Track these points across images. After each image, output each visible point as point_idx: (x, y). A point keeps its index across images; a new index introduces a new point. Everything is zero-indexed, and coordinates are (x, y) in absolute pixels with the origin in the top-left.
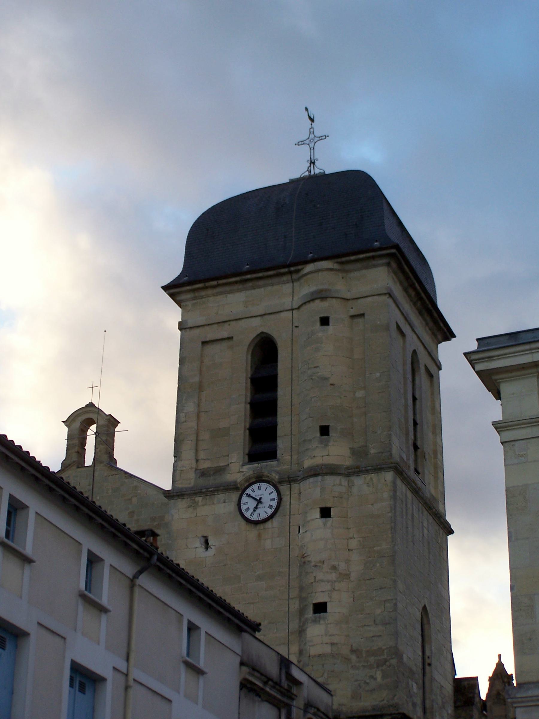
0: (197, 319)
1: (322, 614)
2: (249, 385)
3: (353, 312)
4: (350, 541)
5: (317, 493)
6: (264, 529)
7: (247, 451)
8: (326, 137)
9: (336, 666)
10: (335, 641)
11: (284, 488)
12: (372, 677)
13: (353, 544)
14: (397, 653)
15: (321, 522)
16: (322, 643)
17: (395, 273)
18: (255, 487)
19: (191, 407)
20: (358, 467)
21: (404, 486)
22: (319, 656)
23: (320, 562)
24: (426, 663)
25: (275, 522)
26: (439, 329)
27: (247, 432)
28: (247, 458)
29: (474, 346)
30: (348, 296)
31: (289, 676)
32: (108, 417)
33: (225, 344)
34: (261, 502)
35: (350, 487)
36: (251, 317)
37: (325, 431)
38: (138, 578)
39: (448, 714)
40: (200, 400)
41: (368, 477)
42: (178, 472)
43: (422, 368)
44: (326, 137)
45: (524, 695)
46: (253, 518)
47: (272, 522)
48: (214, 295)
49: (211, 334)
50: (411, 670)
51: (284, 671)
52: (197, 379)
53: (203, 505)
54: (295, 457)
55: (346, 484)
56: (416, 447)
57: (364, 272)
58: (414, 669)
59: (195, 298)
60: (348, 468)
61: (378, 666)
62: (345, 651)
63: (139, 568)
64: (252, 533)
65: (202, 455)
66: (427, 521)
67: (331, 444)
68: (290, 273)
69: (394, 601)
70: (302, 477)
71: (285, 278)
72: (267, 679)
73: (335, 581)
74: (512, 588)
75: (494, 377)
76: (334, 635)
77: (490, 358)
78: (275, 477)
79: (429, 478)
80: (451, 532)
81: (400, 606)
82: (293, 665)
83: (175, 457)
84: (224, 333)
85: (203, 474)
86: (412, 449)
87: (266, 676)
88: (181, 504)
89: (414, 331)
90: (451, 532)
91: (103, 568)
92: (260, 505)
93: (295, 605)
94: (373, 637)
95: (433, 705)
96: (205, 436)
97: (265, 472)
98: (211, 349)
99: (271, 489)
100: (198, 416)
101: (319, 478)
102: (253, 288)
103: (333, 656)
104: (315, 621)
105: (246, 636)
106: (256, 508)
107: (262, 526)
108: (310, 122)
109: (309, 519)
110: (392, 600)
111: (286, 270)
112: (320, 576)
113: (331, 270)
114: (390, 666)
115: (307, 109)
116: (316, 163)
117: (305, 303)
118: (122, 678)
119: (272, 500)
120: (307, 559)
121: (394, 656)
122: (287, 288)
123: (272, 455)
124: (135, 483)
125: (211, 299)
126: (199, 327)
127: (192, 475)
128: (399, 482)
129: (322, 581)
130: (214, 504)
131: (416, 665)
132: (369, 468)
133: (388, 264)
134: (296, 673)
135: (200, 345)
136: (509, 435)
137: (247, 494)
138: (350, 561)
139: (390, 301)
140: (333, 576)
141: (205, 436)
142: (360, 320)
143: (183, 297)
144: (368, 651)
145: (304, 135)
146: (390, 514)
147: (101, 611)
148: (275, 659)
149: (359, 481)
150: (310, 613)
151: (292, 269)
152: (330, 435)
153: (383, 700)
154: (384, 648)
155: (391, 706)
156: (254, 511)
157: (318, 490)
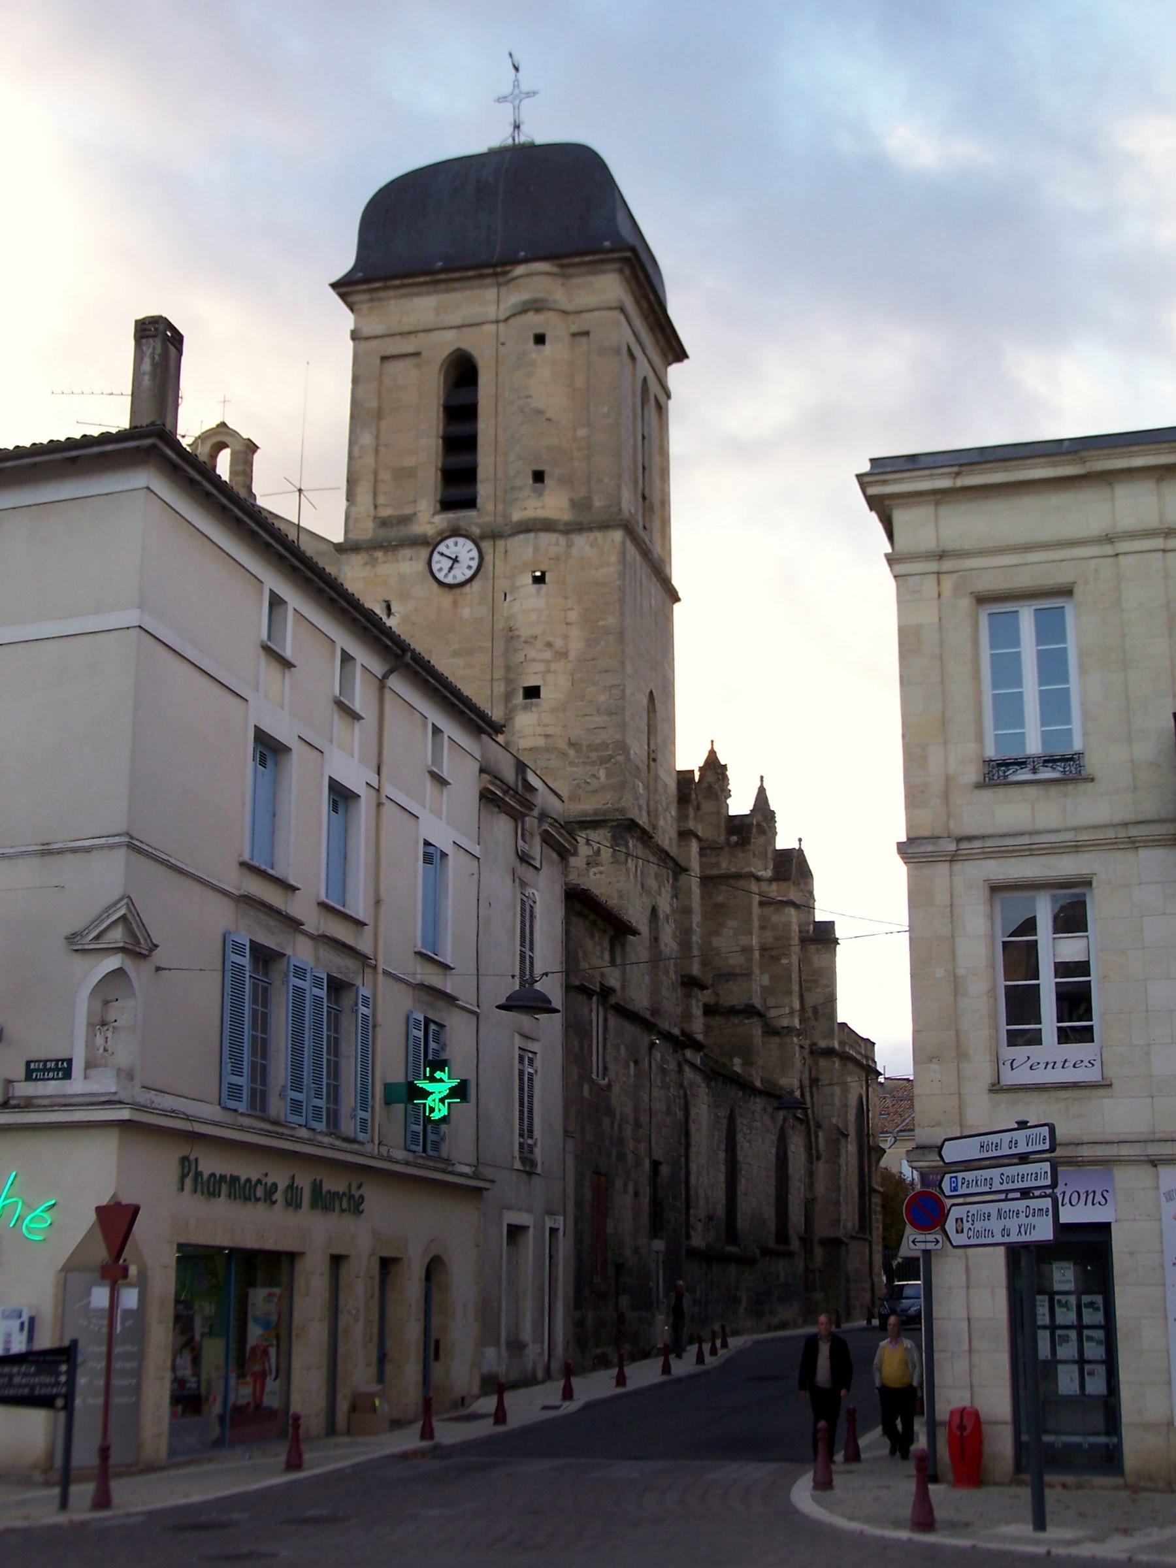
0: (373, 326)
1: (534, 700)
2: (441, 415)
3: (574, 328)
4: (569, 613)
5: (528, 554)
6: (461, 594)
7: (439, 498)
8: (535, 93)
9: (551, 761)
10: (549, 733)
11: (486, 545)
12: (594, 776)
13: (573, 616)
14: (623, 747)
15: (533, 588)
16: (534, 735)
17: (628, 281)
18: (450, 542)
19: (367, 439)
20: (580, 523)
21: (633, 547)
22: (531, 749)
23: (532, 637)
24: (652, 758)
25: (476, 585)
26: (672, 348)
27: (439, 473)
28: (438, 506)
29: (866, 467)
30: (569, 307)
31: (525, 781)
32: (247, 441)
33: (409, 362)
34: (458, 561)
35: (570, 545)
37: (539, 477)
38: (387, 678)
39: (672, 817)
40: (378, 431)
41: (592, 536)
43: (652, 398)
44: (535, 93)
45: (916, 851)
46: (447, 581)
47: (471, 587)
48: (397, 297)
50: (637, 767)
51: (520, 777)
52: (374, 404)
53: (384, 562)
54: (500, 507)
55: (564, 544)
56: (644, 498)
57: (590, 278)
58: (641, 765)
59: (371, 300)
60: (566, 524)
61: (601, 764)
62: (562, 744)
63: (386, 668)
64: (446, 599)
65: (382, 500)
66: (655, 588)
67: (547, 492)
68: (496, 275)
69: (621, 688)
70: (509, 533)
71: (488, 281)
72: (507, 788)
73: (550, 661)
74: (904, 736)
75: (887, 502)
76: (548, 726)
77: (885, 482)
78: (476, 531)
79: (657, 536)
80: (678, 599)
81: (628, 692)
82: (528, 769)
83: (348, 500)
84: (409, 346)
85: (384, 523)
86: (641, 500)
87: (507, 785)
88: (357, 560)
89: (645, 353)
90: (678, 599)
91: (355, 667)
92: (456, 565)
93: (500, 688)
94: (595, 728)
95: (657, 807)
96: (385, 476)
97: (463, 524)
98: (393, 367)
99: (470, 545)
100: (377, 451)
101: (532, 535)
102: (448, 291)
103: (547, 750)
104: (526, 708)
105: (484, 737)
106: (451, 568)
107: (458, 591)
108: (513, 71)
109: (518, 584)
110: (619, 685)
111: (491, 271)
112: (532, 654)
113: (549, 274)
114: (615, 764)
115: (511, 55)
116: (522, 127)
117: (514, 315)
118: (373, 793)
119: (472, 559)
120: (517, 633)
121: (621, 752)
122: (491, 294)
123: (470, 503)
125: (393, 302)
126: (376, 337)
127: (370, 525)
128: (629, 544)
129: (534, 660)
130: (397, 561)
131: (642, 761)
132: (592, 525)
133: (621, 271)
134: (532, 779)
135: (378, 361)
136: (902, 568)
137: (439, 553)
139: (622, 318)
140: (548, 655)
141: (385, 476)
142: (584, 340)
143: (354, 298)
144: (589, 746)
145: (507, 89)
146: (618, 583)
147: (354, 718)
148: (512, 761)
149: (581, 541)
150: (519, 698)
151: (499, 270)
152: (546, 482)
153: (608, 803)
154: (609, 742)
155: (618, 810)
156: (449, 572)
157: (531, 550)
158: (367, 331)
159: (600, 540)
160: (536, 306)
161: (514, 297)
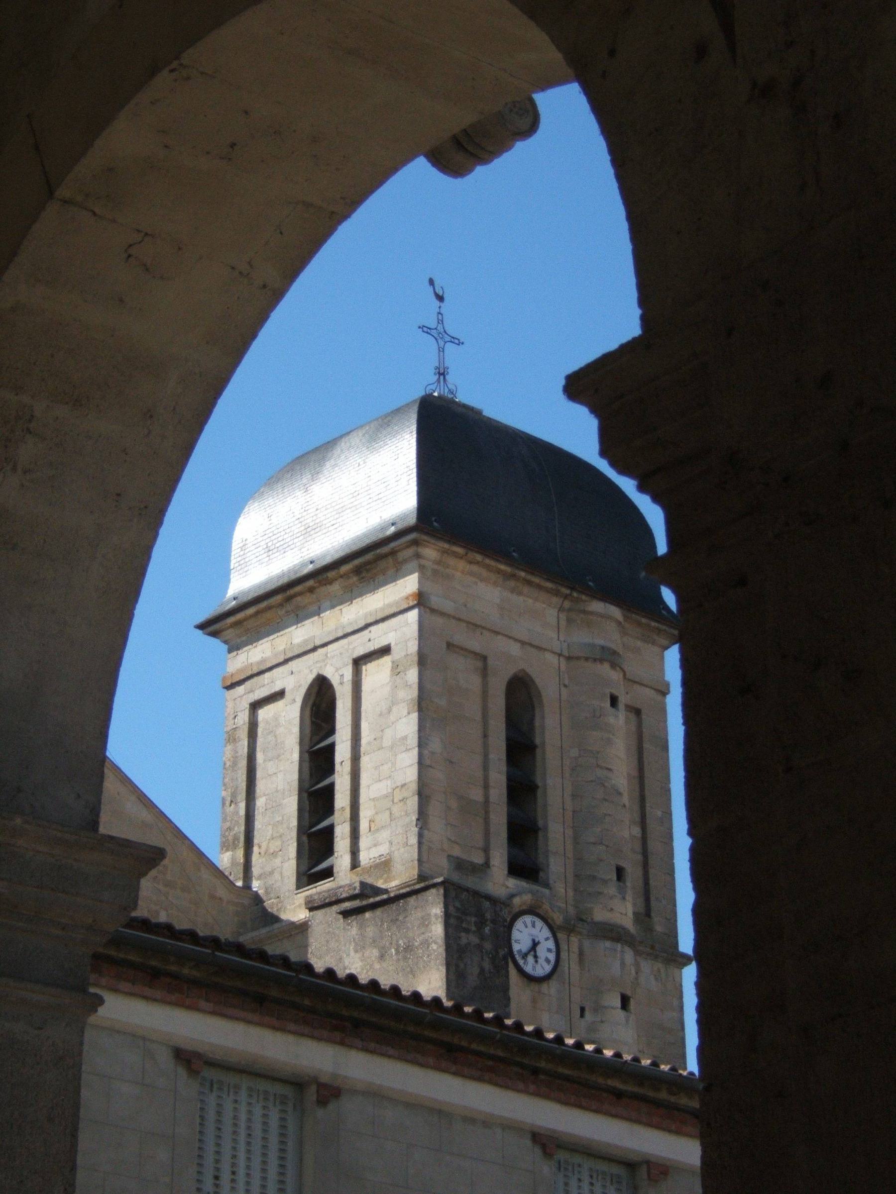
19: (436, 745)
36: (510, 638)
42: (425, 848)
44: (460, 343)
49: (461, 637)
78: (558, 918)
99: (546, 932)
101: (619, 946)
107: (534, 986)
108: (437, 303)
115: (431, 282)
158: (435, 601)
160: (609, 657)
161: (582, 637)
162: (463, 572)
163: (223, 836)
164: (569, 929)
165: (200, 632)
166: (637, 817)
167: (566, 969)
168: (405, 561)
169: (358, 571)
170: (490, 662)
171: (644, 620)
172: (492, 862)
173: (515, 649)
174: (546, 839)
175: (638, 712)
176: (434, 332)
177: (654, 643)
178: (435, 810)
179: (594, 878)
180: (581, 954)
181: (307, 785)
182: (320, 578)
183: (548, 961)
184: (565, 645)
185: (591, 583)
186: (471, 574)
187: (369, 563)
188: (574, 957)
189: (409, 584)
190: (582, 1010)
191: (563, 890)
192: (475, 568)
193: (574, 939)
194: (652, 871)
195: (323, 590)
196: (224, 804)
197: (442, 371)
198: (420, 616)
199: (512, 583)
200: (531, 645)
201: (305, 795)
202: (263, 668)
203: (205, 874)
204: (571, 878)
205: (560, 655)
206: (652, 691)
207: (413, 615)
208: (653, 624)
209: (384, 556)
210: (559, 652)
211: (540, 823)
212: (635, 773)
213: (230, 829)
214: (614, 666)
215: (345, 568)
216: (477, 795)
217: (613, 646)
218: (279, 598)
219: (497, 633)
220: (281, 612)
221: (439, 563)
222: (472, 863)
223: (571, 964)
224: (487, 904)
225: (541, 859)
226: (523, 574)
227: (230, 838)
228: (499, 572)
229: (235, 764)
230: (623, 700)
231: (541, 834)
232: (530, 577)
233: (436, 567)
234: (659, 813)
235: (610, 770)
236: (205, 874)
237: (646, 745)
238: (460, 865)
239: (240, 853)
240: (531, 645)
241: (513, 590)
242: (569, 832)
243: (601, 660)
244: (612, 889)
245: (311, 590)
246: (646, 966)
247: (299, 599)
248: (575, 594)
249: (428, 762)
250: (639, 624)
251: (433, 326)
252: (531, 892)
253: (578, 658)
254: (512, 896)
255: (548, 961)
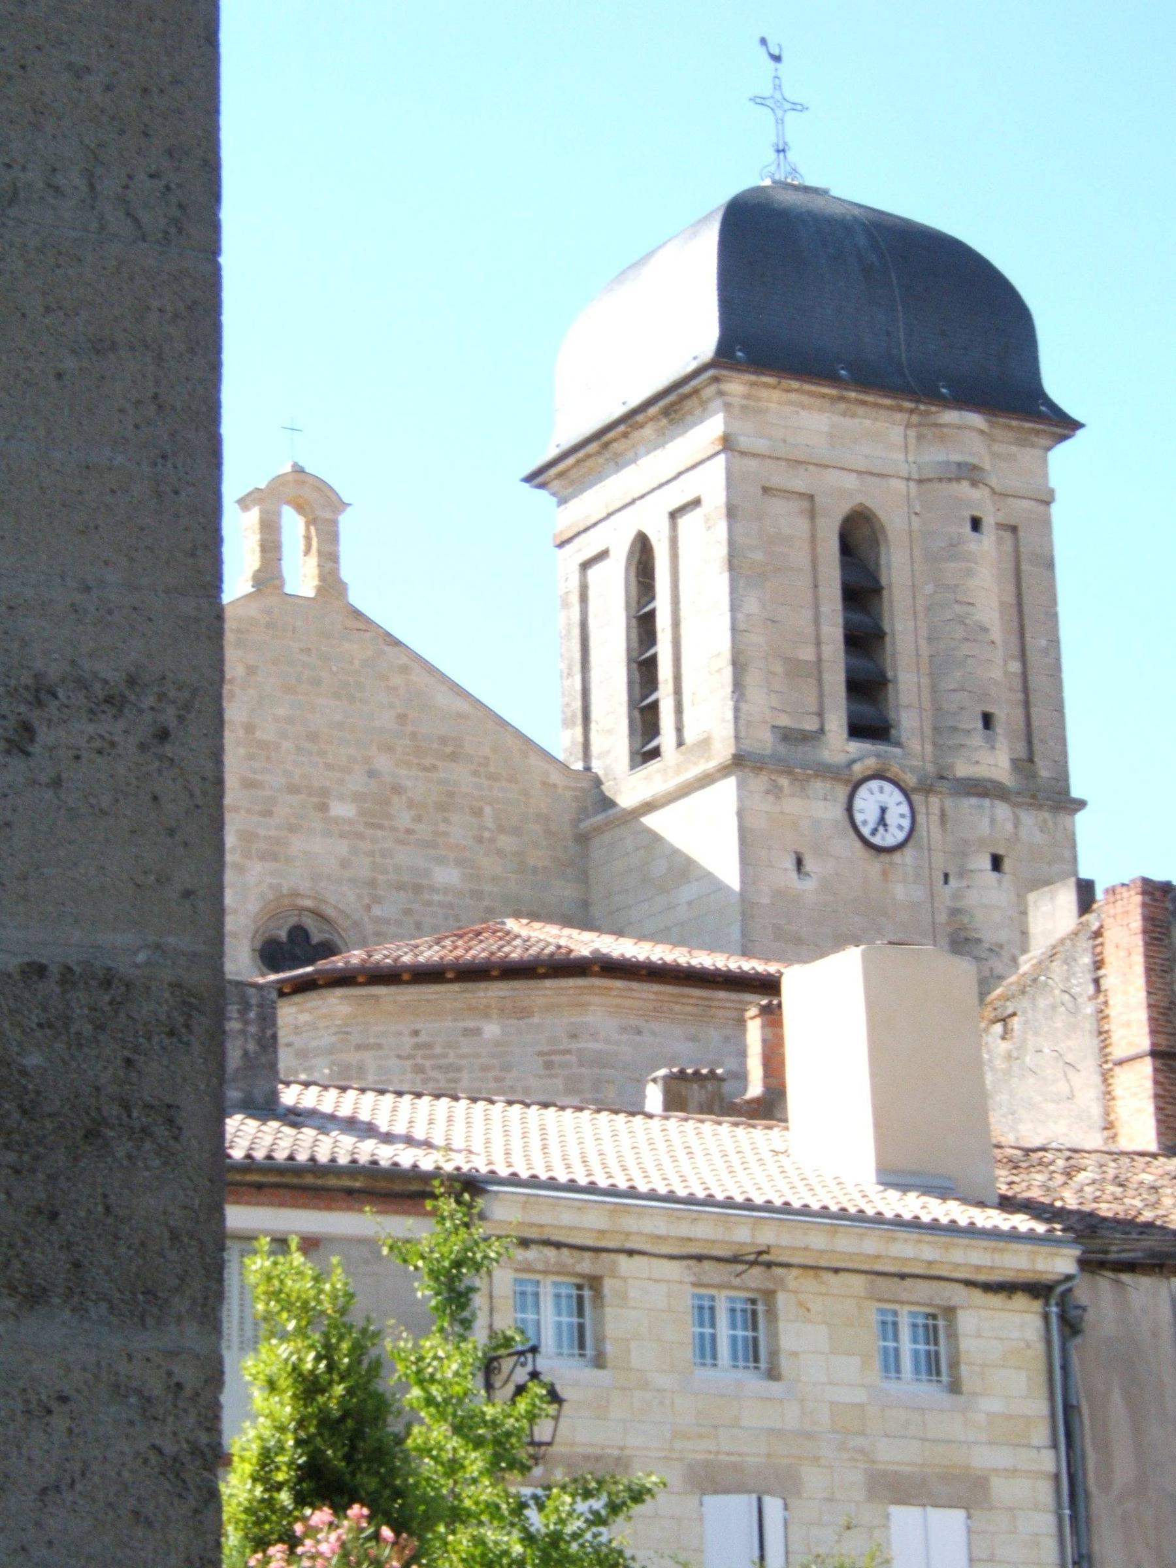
19: (751, 605)
36: (843, 469)
42: (742, 722)
44: (804, 108)
49: (780, 478)
64: (874, 866)
78: (911, 780)
99: (898, 796)
101: (987, 802)
107: (885, 858)
108: (772, 64)
115: (763, 41)
124: (404, 660)
138: (1075, 960)
158: (744, 443)
159: (1050, 824)
160: (970, 473)
161: (935, 455)
162: (779, 403)
163: (564, 712)
164: (926, 789)
165: (526, 485)
166: (1016, 651)
167: (925, 834)
168: (709, 400)
169: (666, 412)
170: (818, 500)
171: (1014, 423)
172: (827, 728)
173: (850, 482)
174: (897, 691)
175: (1014, 529)
176: (770, 102)
177: (1033, 446)
178: (753, 679)
179: (955, 729)
180: (943, 815)
181: (635, 654)
182: (630, 422)
183: (900, 827)
184: (914, 468)
185: (944, 391)
186: (790, 403)
187: (673, 404)
188: (935, 818)
189: (712, 427)
190: (946, 876)
191: (919, 747)
192: (793, 397)
193: (934, 800)
194: (1034, 711)
195: (637, 435)
196: (562, 677)
197: (781, 147)
198: (728, 461)
199: (842, 406)
200: (871, 474)
201: (635, 666)
202: (589, 524)
203: (534, 760)
204: (928, 731)
205: (908, 479)
206: (1032, 503)
207: (722, 458)
208: (1028, 425)
209: (687, 396)
210: (906, 476)
211: (890, 675)
212: (1012, 600)
213: (568, 705)
214: (974, 483)
215: (653, 411)
216: (807, 653)
217: (974, 460)
218: (593, 447)
219: (826, 467)
220: (601, 460)
221: (747, 397)
222: (802, 732)
223: (930, 828)
224: (252, 991)
225: (892, 715)
226: (853, 395)
227: (569, 714)
228: (823, 396)
229: (569, 632)
230: (988, 522)
231: (890, 686)
232: (862, 397)
233: (745, 402)
234: (1043, 643)
235: (972, 604)
236: (534, 760)
237: (1025, 567)
238: (788, 736)
239: (579, 730)
240: (871, 474)
241: (844, 414)
242: (925, 681)
243: (958, 479)
244: (978, 738)
245: (625, 435)
246: (1029, 819)
247: (615, 445)
248: (922, 407)
249: (742, 626)
250: (1010, 428)
251: (767, 94)
252: (878, 756)
253: (930, 480)
254: (854, 761)
255: (900, 827)
